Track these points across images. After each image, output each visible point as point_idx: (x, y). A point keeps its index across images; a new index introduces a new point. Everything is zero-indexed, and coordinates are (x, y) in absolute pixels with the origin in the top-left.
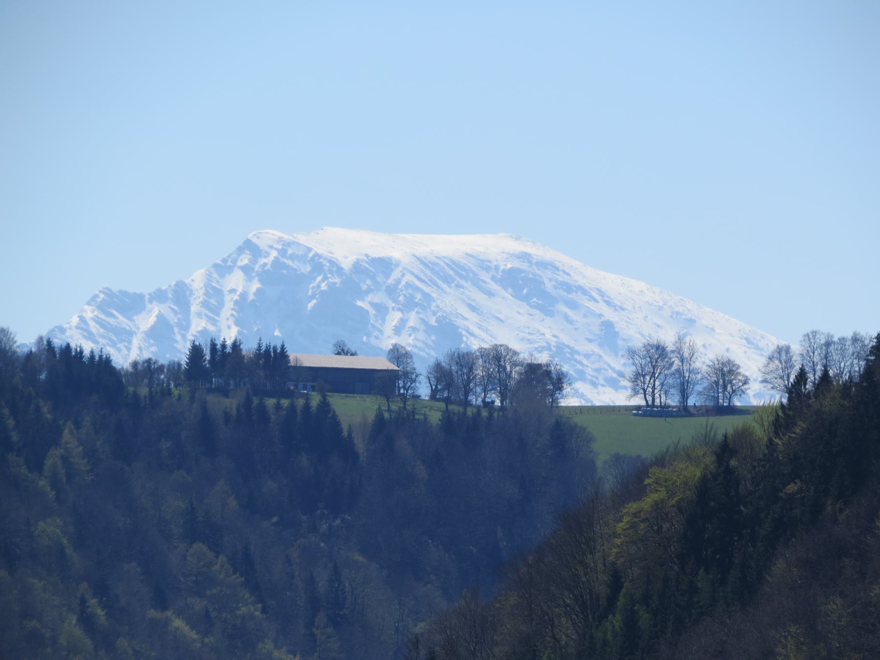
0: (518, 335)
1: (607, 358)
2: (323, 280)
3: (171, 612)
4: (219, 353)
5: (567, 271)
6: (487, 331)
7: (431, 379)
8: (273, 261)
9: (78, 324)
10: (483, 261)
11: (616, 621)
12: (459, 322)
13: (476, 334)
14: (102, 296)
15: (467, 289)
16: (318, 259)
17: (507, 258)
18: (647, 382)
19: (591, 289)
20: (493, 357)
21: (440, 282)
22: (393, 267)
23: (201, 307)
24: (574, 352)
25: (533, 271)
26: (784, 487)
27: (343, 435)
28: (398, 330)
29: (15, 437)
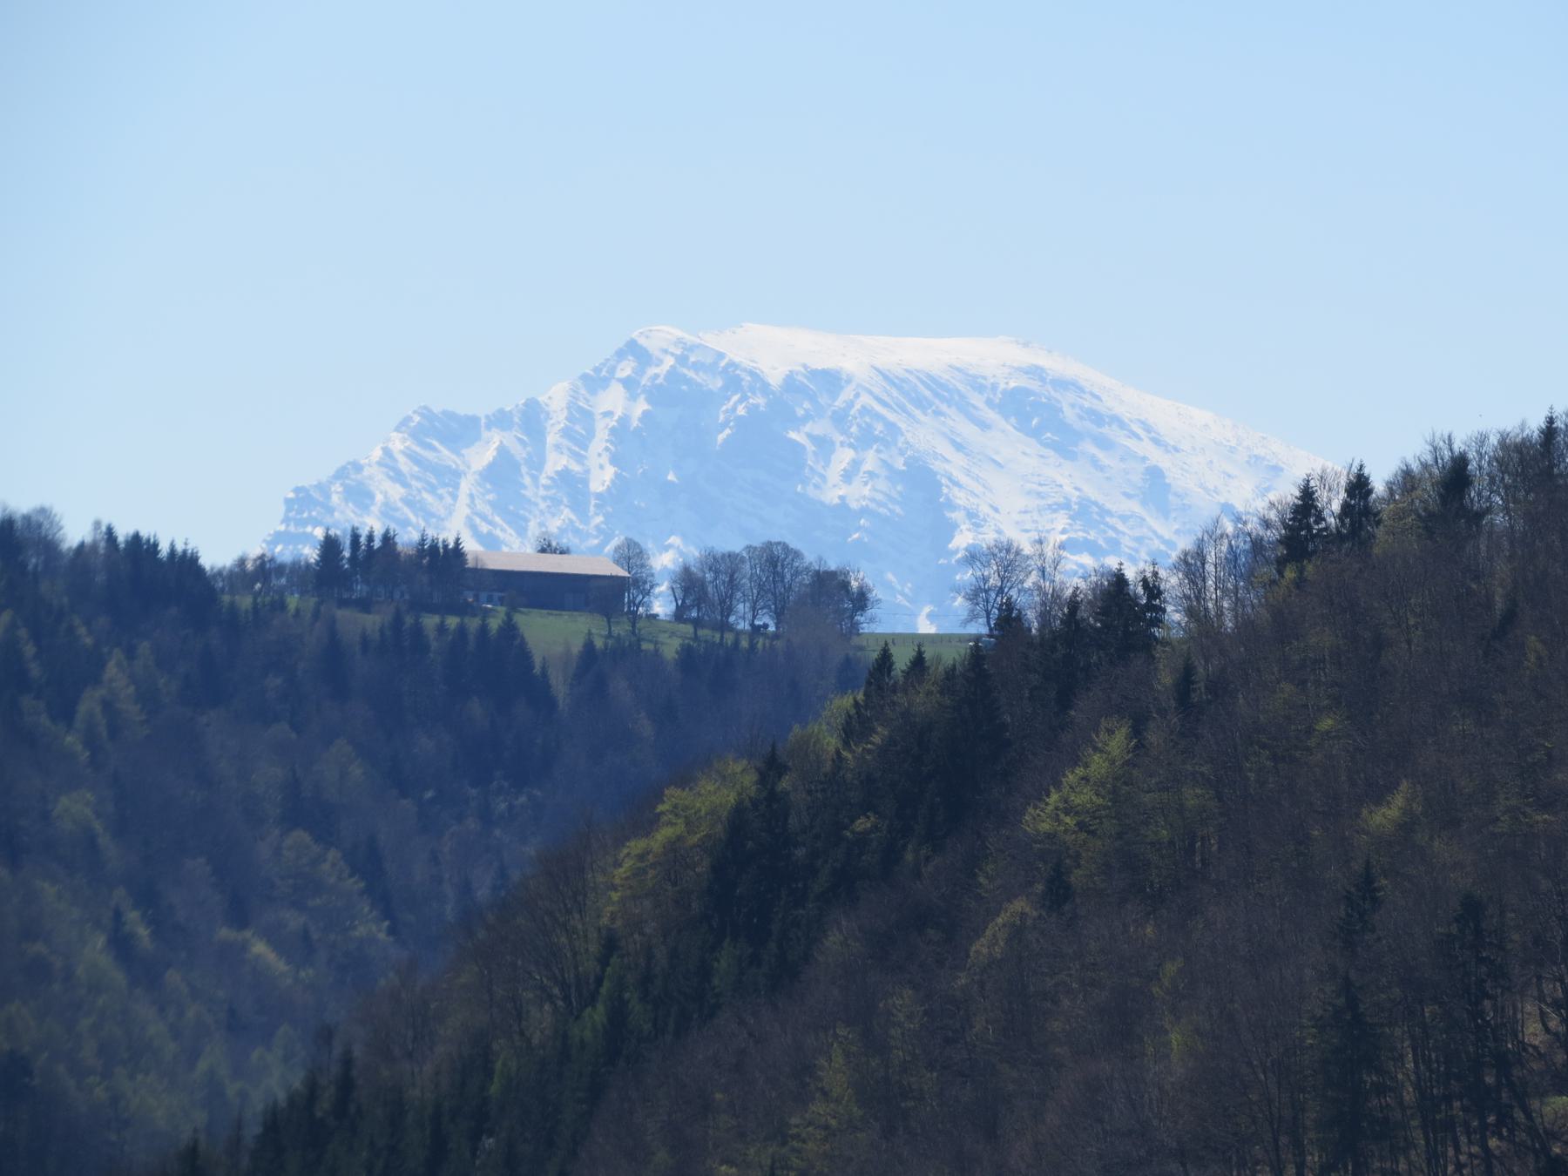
0: (1022, 486)
1: (1151, 521)
2: (740, 401)
4: (363, 547)
5: (1098, 394)
6: (977, 479)
7: (675, 590)
8: (668, 371)
9: (380, 458)
10: (975, 377)
11: (598, 1015)
12: (937, 466)
13: (961, 483)
14: (417, 418)
15: (950, 417)
16: (734, 371)
17: (1010, 374)
18: (991, 600)
19: (1131, 421)
20: (766, 561)
21: (910, 407)
22: (843, 383)
23: (561, 436)
24: (1104, 512)
25: (1046, 393)
26: (853, 822)
27: (534, 671)
28: (848, 476)
29: (35, 670)
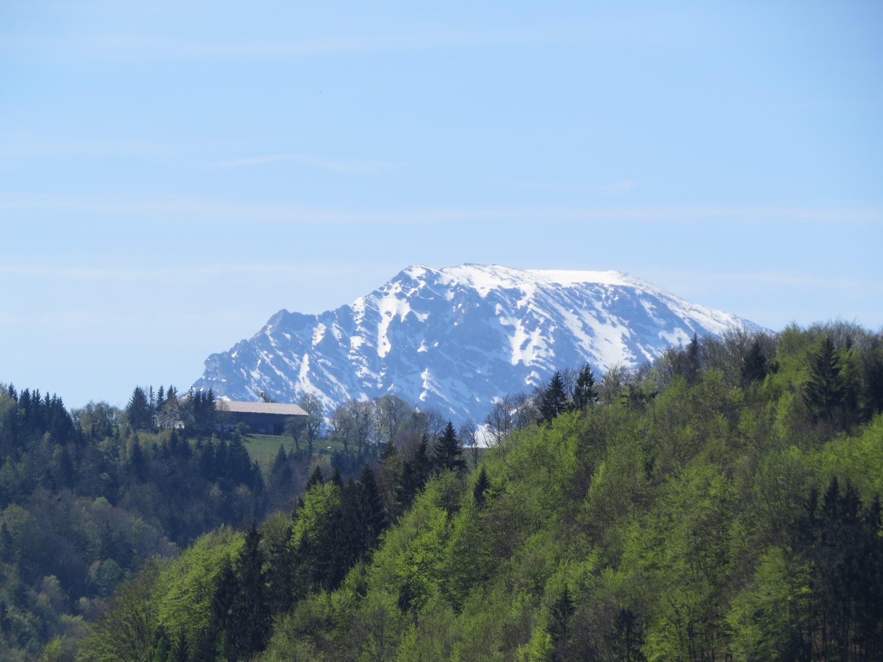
3: (82, 617)
28: (523, 347)
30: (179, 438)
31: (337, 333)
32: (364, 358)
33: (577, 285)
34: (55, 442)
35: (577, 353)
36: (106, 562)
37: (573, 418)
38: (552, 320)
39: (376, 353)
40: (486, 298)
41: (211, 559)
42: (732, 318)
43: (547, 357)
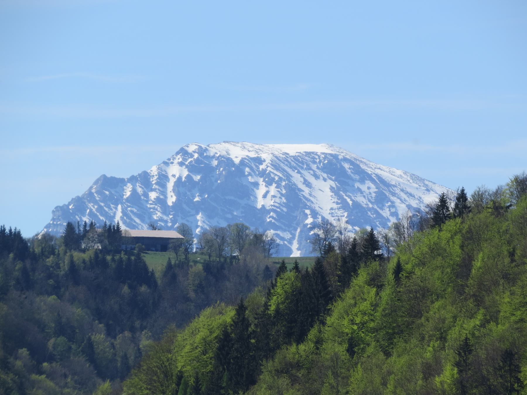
28: (265, 196)
30: (100, 255)
31: (140, 190)
32: (158, 206)
33: (299, 154)
34: (17, 259)
35: (301, 199)
36: (59, 339)
37: (457, 223)
38: (284, 178)
39: (166, 203)
40: (239, 164)
41: (213, 324)
42: (404, 173)
43: (281, 203)
